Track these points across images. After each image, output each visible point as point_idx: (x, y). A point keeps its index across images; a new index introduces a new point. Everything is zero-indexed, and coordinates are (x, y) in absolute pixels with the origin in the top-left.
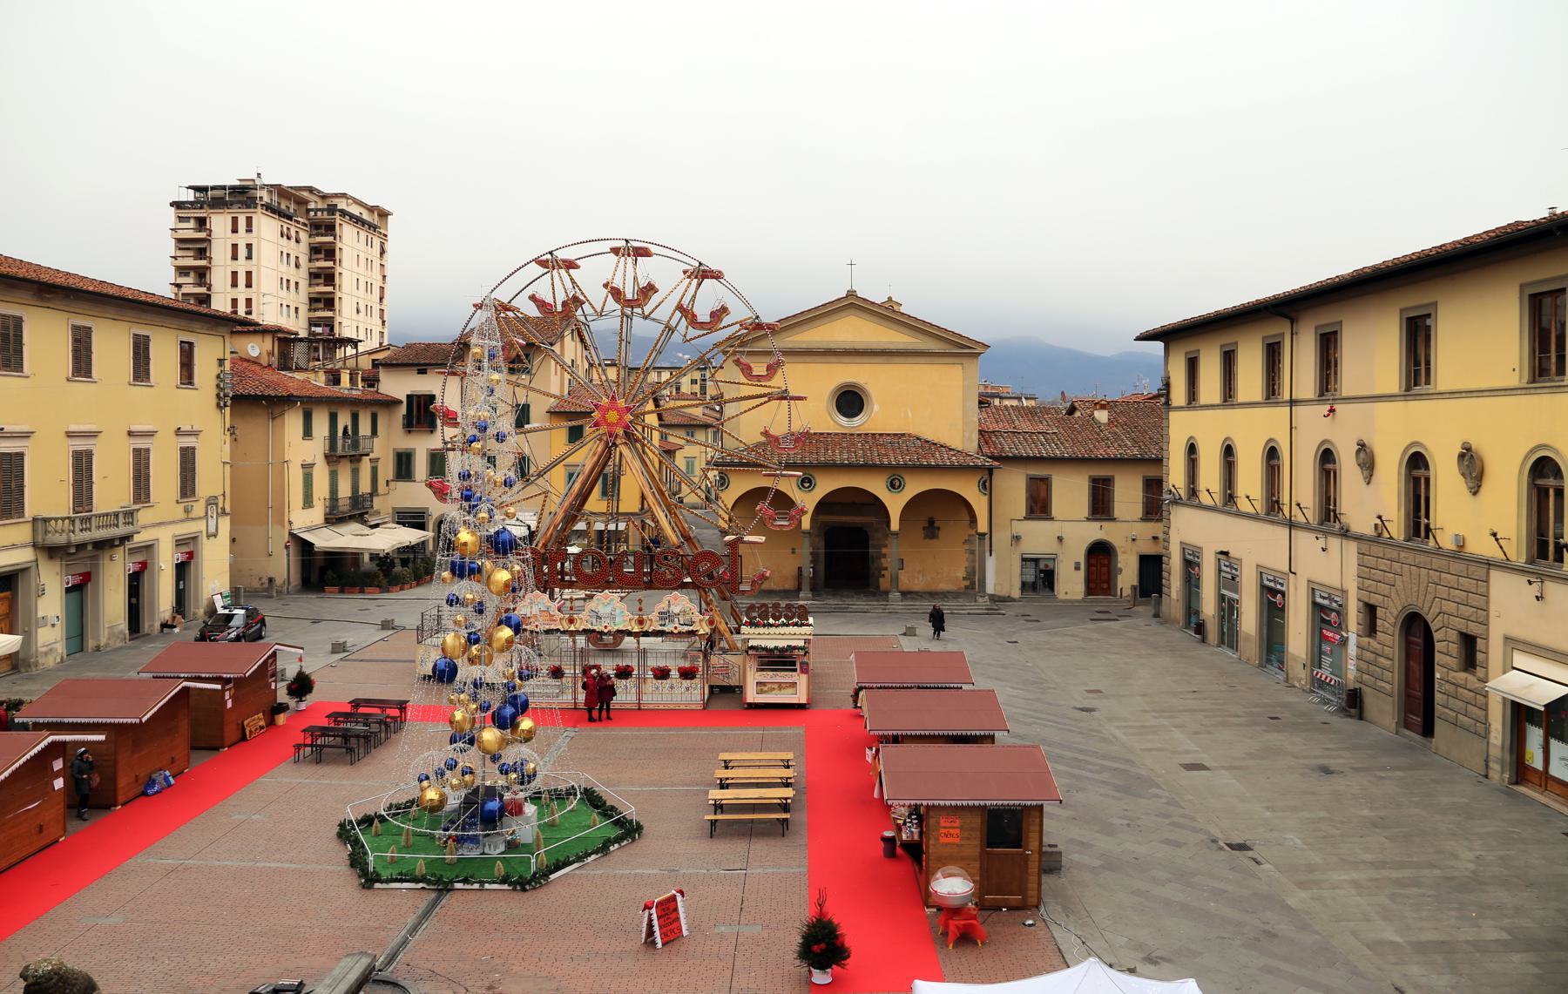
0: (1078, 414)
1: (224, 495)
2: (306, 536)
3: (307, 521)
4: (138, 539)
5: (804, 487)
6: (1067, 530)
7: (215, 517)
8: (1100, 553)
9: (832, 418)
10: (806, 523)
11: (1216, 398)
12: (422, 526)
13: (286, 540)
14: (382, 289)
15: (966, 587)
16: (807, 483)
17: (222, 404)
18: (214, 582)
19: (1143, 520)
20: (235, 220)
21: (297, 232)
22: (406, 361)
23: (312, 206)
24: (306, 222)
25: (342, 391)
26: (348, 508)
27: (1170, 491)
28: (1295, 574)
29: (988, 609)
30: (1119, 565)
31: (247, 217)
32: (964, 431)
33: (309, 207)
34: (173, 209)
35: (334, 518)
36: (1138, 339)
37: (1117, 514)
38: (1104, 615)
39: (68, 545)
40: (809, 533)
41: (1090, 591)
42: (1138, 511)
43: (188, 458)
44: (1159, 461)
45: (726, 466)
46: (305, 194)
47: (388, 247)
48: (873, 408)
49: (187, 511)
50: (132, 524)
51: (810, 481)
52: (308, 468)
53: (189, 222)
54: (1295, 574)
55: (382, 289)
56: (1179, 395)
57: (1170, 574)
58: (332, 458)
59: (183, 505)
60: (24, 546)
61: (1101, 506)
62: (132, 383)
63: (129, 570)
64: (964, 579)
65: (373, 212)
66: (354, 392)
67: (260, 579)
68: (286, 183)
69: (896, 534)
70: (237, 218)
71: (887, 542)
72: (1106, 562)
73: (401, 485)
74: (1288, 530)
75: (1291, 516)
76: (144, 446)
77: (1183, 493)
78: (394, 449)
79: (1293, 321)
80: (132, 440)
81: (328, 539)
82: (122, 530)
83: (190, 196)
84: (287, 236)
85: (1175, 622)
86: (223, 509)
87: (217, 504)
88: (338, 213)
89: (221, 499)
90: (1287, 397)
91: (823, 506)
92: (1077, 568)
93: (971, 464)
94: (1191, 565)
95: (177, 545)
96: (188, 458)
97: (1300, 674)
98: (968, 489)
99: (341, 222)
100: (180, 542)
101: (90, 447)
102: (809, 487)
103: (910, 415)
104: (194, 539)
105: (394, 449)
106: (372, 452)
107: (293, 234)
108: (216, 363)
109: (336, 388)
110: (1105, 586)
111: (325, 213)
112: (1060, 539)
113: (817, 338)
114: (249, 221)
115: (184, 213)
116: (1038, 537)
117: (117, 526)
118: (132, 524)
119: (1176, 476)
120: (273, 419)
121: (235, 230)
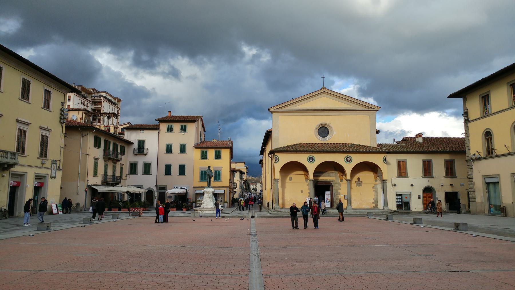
1: (60, 161)
3: (96, 181)
4: (16, 169)
5: (310, 161)
7: (55, 170)
8: (428, 191)
9: (316, 137)
13: (86, 187)
15: (374, 207)
17: (62, 121)
19: (445, 177)
21: (87, 103)
23: (93, 95)
24: (91, 100)
30: (437, 197)
32: (371, 142)
33: (92, 95)
35: (105, 183)
37: (434, 175)
43: (44, 140)
46: (91, 90)
49: (43, 164)
50: (15, 159)
51: (312, 159)
52: (96, 159)
62: (20, 99)
63: (11, 184)
64: (373, 203)
65: (115, 100)
72: (430, 195)
73: (132, 176)
78: (129, 162)
80: (18, 124)
82: (9, 160)
84: (84, 104)
86: (59, 167)
87: (56, 164)
92: (419, 198)
95: (36, 179)
96: (44, 140)
99: (104, 101)
100: (38, 177)
102: (312, 161)
104: (44, 177)
105: (129, 162)
107: (86, 104)
117: (7, 158)
118: (15, 159)
120: (83, 137)
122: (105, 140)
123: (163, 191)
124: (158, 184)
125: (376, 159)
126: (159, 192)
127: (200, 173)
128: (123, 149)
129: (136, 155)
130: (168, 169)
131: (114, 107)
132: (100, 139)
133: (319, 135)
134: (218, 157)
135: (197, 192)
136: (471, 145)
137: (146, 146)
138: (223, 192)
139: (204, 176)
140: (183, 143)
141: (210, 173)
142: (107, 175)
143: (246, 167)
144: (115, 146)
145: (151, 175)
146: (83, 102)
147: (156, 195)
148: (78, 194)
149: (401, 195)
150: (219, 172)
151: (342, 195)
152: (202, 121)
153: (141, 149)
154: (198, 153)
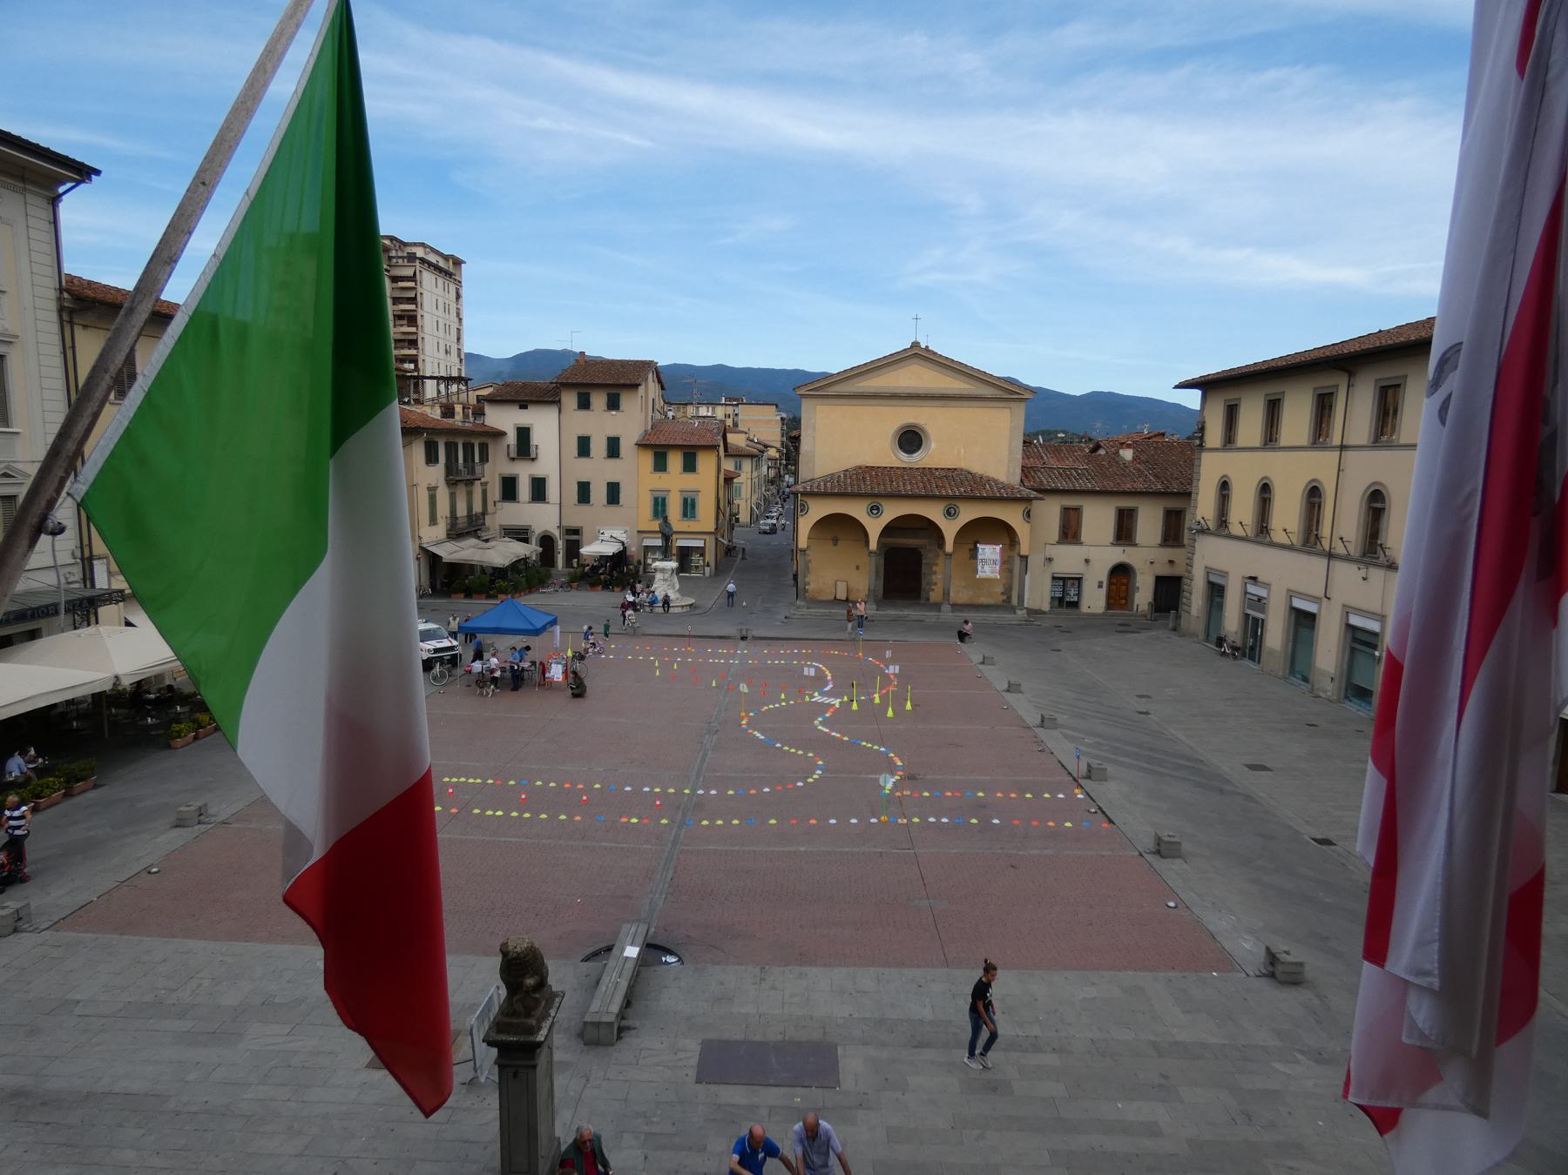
0: (1102, 452)
2: (430, 549)
3: (433, 535)
6: (1093, 553)
8: (1121, 573)
10: (873, 545)
11: (1257, 440)
12: (526, 541)
13: (418, 552)
14: (459, 330)
15: (1003, 601)
16: (875, 510)
22: (509, 398)
26: (466, 525)
27: (1199, 522)
28: (1329, 599)
29: (1026, 621)
30: (1137, 585)
35: (455, 533)
36: (1177, 387)
38: (1125, 628)
40: (875, 553)
41: (1109, 606)
42: (1158, 538)
44: (1187, 495)
47: (464, 292)
48: (930, 445)
51: (878, 509)
52: (432, 490)
54: (1329, 599)
55: (459, 330)
56: (1214, 435)
57: (1191, 594)
58: (452, 482)
61: (1124, 532)
64: (1002, 594)
65: (448, 261)
66: (467, 424)
71: (937, 561)
72: (1125, 581)
73: (508, 506)
74: (1326, 561)
75: (1330, 548)
77: (1212, 525)
79: (1351, 374)
81: (451, 552)
85: (1193, 635)
88: (418, 261)
90: (1336, 441)
91: (889, 530)
92: (1100, 586)
93: (1019, 496)
94: (1216, 591)
97: (1329, 689)
98: (1011, 515)
103: (962, 452)
106: (484, 477)
109: (450, 421)
110: (1123, 602)
111: (406, 260)
112: (1087, 561)
116: (1068, 559)
119: (1204, 506)
123: (575, 537)
124: (563, 524)
126: (567, 540)
127: (653, 502)
129: (513, 459)
130: (584, 492)
131: (447, 282)
132: (437, 443)
133: (901, 448)
134: (689, 466)
136: (1199, 497)
137: (536, 439)
138: (700, 544)
139: (660, 508)
141: (667, 530)
142: (457, 518)
143: (779, 418)
144: (468, 448)
145: (548, 503)
147: (560, 547)
150: (693, 501)
151: (939, 577)
153: (524, 445)
154: (648, 459)
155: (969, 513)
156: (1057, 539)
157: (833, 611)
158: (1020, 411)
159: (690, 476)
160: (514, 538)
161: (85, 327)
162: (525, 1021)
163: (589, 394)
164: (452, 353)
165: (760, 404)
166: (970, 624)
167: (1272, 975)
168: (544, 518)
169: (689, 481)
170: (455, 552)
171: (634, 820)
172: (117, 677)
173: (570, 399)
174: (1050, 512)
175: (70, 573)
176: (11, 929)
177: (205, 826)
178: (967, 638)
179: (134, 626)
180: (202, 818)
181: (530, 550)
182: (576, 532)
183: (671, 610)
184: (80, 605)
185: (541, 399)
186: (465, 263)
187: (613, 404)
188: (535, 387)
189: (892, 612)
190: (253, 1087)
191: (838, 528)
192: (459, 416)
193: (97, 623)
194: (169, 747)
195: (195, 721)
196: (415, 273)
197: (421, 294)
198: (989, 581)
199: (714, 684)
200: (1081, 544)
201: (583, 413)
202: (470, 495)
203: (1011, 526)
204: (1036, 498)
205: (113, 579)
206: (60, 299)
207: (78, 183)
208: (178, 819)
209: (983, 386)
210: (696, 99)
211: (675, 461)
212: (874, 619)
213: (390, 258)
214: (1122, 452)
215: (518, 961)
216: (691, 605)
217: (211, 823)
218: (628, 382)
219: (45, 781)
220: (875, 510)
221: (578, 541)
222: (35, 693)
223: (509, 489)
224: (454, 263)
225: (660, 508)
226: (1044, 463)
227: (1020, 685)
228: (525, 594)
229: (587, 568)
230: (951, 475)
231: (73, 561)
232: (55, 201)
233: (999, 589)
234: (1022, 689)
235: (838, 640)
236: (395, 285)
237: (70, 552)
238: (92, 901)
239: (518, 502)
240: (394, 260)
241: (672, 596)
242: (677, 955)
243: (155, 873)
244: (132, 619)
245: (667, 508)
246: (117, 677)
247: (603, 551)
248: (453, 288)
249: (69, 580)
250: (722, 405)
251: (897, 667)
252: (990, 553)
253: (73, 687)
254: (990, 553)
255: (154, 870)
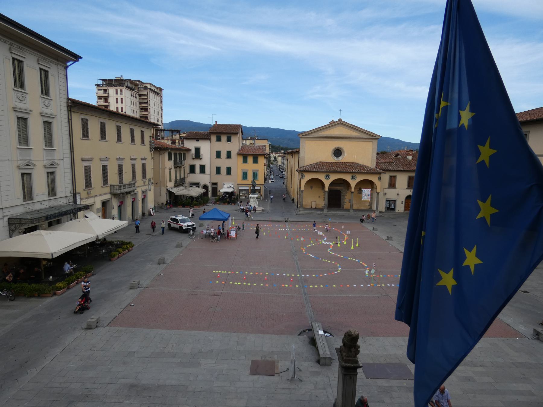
1: (152, 178)
2: (171, 190)
3: (170, 185)
6: (400, 192)
9: (332, 157)
10: (327, 189)
14: (161, 113)
15: (369, 208)
16: (327, 177)
18: (151, 205)
20: (117, 91)
21: (136, 95)
25: (176, 146)
29: (379, 215)
31: (121, 90)
34: (96, 86)
35: (177, 185)
39: (120, 193)
43: (144, 166)
45: (302, 172)
46: (138, 82)
47: (163, 100)
50: (134, 187)
51: (328, 176)
52: (170, 169)
53: (101, 91)
55: (161, 113)
58: (175, 167)
59: (143, 181)
60: (106, 194)
64: (369, 206)
65: (158, 89)
66: (180, 147)
67: (158, 203)
68: (132, 79)
69: (352, 192)
70: (117, 90)
71: (347, 195)
73: (192, 175)
76: (134, 163)
81: (178, 191)
82: (132, 189)
83: (100, 82)
86: (152, 183)
87: (150, 181)
88: (148, 89)
89: (151, 179)
92: (402, 203)
98: (374, 179)
101: (122, 163)
103: (356, 157)
105: (189, 164)
107: (135, 95)
108: (149, 137)
109: (174, 145)
112: (398, 194)
113: (329, 133)
114: (121, 91)
115: (99, 88)
116: (391, 194)
121: (117, 93)
122: (174, 153)
123: (215, 186)
124: (211, 181)
125: (374, 179)
128: (184, 154)
129: (194, 159)
134: (255, 161)
135: (241, 188)
137: (202, 152)
139: (245, 176)
140: (229, 150)
143: (269, 144)
144: (180, 154)
145: (206, 174)
146: (132, 94)
148: (161, 196)
149: (390, 201)
150: (257, 174)
152: (242, 129)
153: (197, 154)
154: (241, 159)
155: (360, 178)
156: (388, 187)
157: (312, 212)
158: (376, 142)
159: (255, 165)
160: (197, 186)
161: (74, 112)
162: (354, 359)
163: (220, 136)
164: (159, 122)
165: (259, 139)
166: (365, 216)
167: (538, 339)
168: (204, 179)
169: (255, 167)
170: (178, 191)
171: (287, 286)
172: (97, 236)
173: (214, 138)
174: (386, 177)
175: (69, 199)
176: (95, 326)
177: (141, 289)
178: (363, 221)
179: (87, 217)
180: (139, 286)
181: (200, 191)
182: (216, 184)
183: (256, 212)
184: (72, 212)
185: (203, 138)
186: (163, 90)
187: (229, 140)
188: (200, 134)
189: (333, 212)
190: (215, 382)
191: (315, 183)
192: (177, 144)
193: (77, 218)
194: (110, 260)
195: (118, 251)
196: (147, 93)
197: (149, 101)
198: (365, 201)
199: (286, 238)
200: (396, 188)
201: (218, 143)
202: (180, 171)
203: (324, 183)
204: (383, 173)
205: (81, 201)
206: (67, 102)
207: (75, 61)
208: (131, 286)
209: (365, 135)
210: (236, 34)
211: (250, 160)
212: (327, 214)
213: (139, 88)
214: (408, 157)
215: (356, 338)
216: (262, 210)
217: (142, 288)
218: (234, 132)
219: (78, 273)
220: (327, 177)
221: (216, 187)
222: (76, 242)
223: (192, 169)
224: (160, 90)
225: (245, 176)
226: (379, 161)
227: (392, 238)
228: (202, 206)
229: (221, 197)
230: (352, 165)
231: (71, 195)
232: (66, 68)
233: (368, 204)
234: (393, 239)
235: (319, 222)
236: (140, 98)
237: (69, 192)
238: (117, 316)
239: (195, 174)
240: (140, 89)
241: (257, 207)
242: (329, 333)
243: (133, 305)
244: (87, 215)
245: (242, 176)
246: (97, 236)
247: (227, 191)
248: (159, 98)
249: (70, 201)
250: (249, 140)
251: (349, 232)
252: (366, 192)
253: (86, 240)
254: (366, 192)
255: (132, 304)
